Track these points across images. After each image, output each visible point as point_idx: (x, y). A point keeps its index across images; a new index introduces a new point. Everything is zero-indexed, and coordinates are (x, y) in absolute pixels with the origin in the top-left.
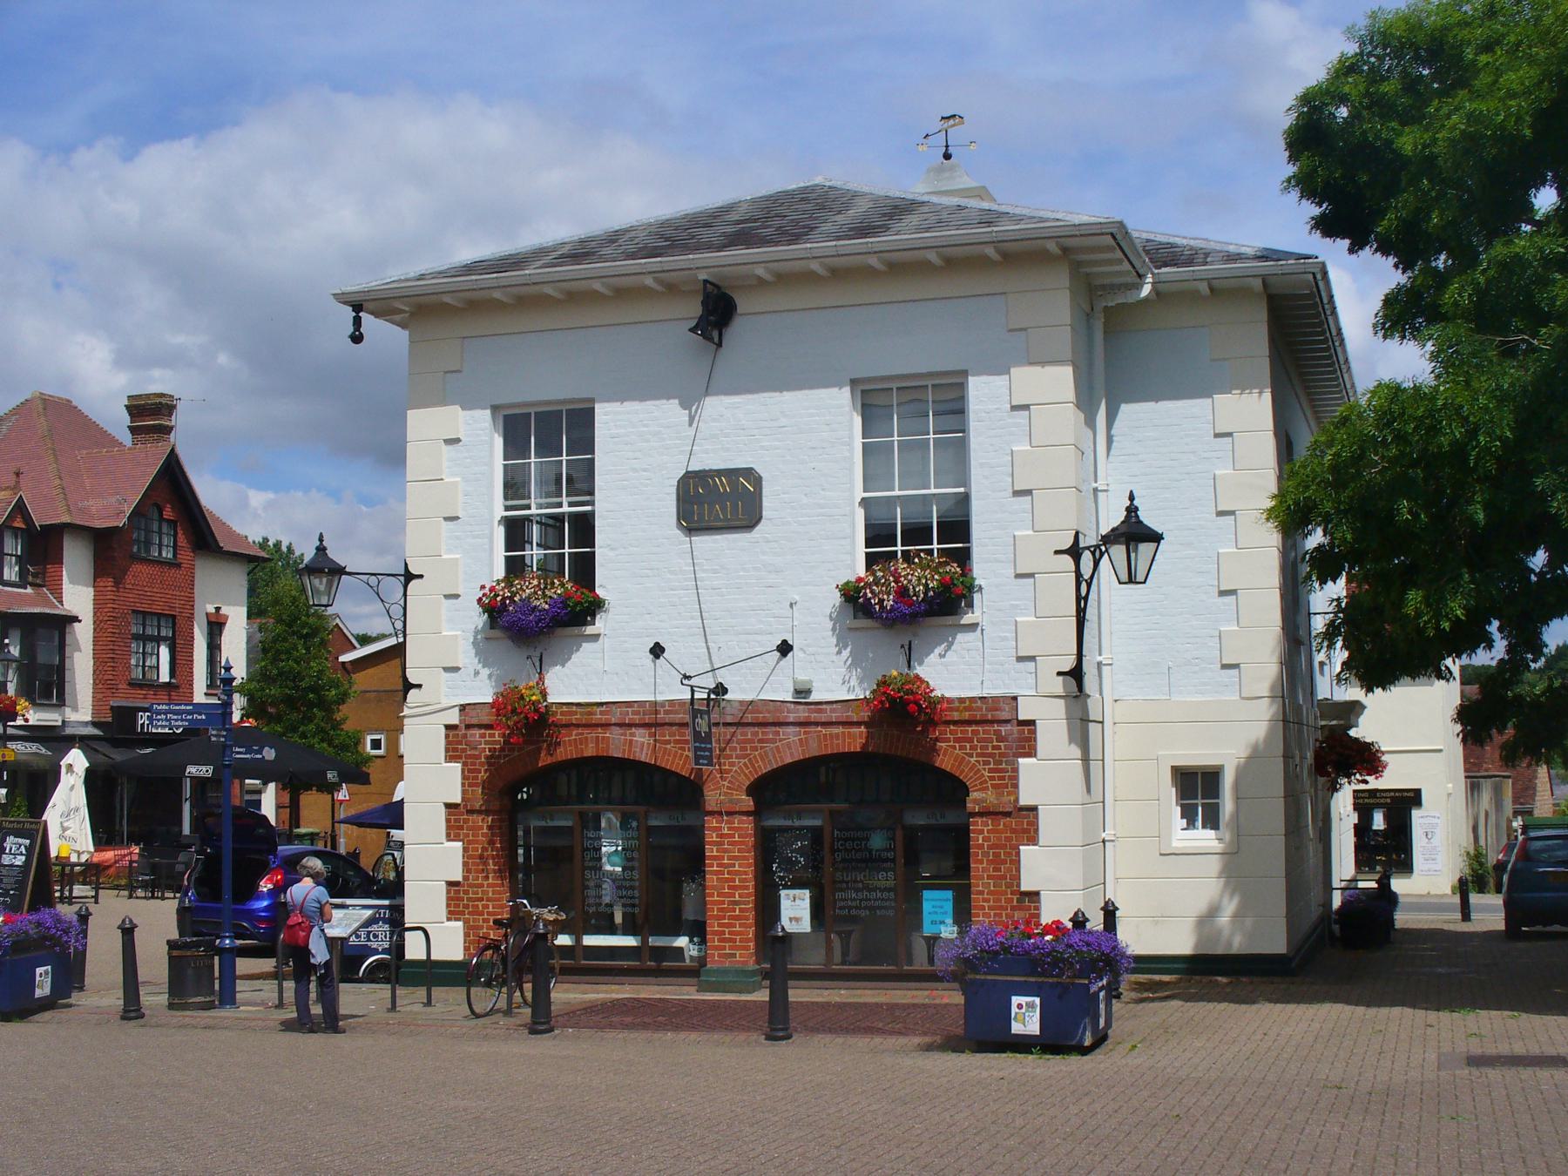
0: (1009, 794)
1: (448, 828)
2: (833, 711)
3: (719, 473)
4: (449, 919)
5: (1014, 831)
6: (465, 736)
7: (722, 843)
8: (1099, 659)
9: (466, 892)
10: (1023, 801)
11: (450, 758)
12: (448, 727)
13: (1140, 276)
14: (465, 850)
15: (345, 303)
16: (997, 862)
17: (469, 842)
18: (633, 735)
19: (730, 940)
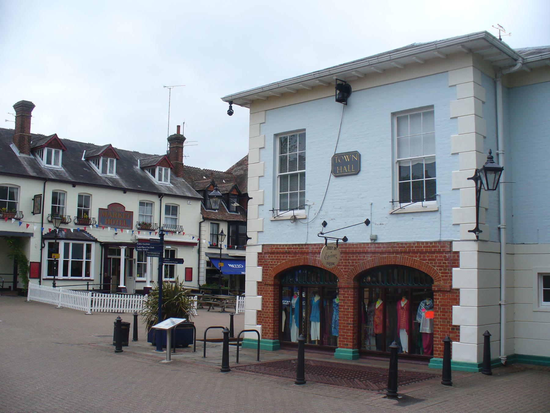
3: (346, 154)
5: (451, 299)
6: (264, 257)
8: (499, 226)
13: (516, 60)
14: (263, 299)
15: (226, 101)
16: (444, 312)
17: (265, 296)
18: (316, 257)
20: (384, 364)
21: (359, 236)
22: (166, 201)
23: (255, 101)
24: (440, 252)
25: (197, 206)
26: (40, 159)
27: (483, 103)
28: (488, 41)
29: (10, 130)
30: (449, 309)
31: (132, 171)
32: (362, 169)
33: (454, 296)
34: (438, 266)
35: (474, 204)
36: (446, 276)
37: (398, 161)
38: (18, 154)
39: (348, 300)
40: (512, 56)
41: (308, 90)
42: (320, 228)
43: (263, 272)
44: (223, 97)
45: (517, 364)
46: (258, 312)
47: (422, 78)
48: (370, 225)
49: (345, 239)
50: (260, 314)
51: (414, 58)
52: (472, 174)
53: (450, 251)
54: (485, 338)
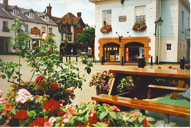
15: (93, 2)
22: (49, 27)
25: (57, 28)
26: (12, 13)
29: (2, 4)
31: (38, 18)
33: (149, 48)
38: (5, 11)
49: (122, 36)
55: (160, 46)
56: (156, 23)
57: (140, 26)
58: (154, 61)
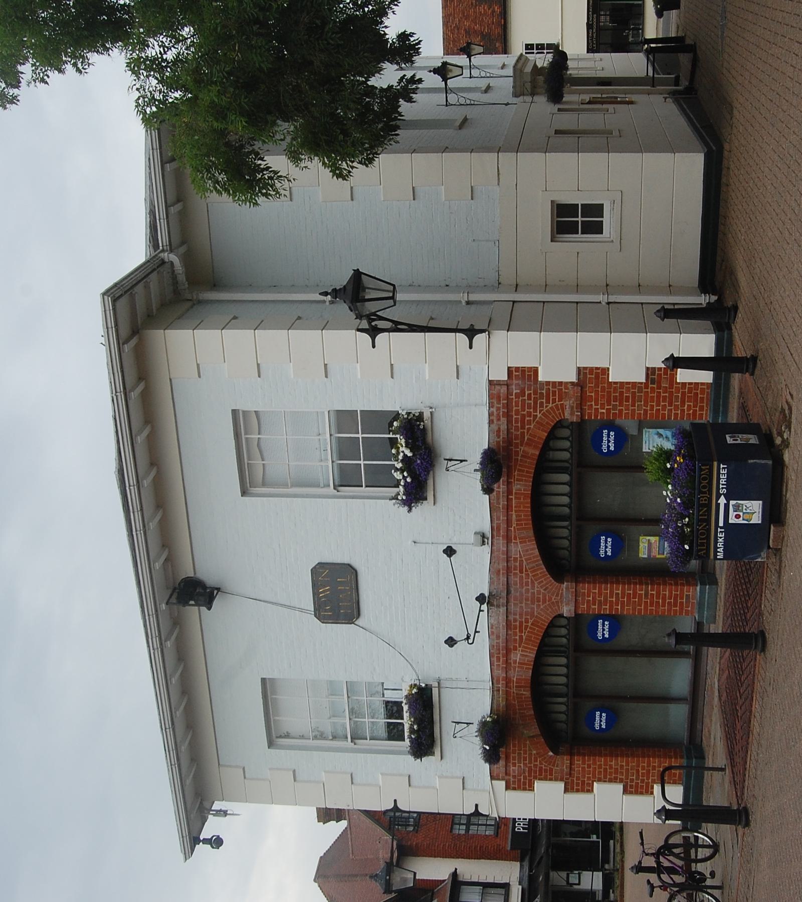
0: (566, 388)
1: (583, 791)
2: (498, 519)
3: (315, 593)
4: (652, 793)
5: (597, 386)
6: (514, 777)
7: (600, 602)
8: (464, 303)
9: (632, 780)
10: (574, 379)
11: (531, 788)
12: (507, 788)
13: (163, 262)
14: (599, 780)
15: (192, 851)
16: (621, 399)
17: (594, 776)
18: (515, 662)
19: (676, 599)
20: (714, 657)
21: (477, 570)
23: (197, 798)
24: (508, 406)
27: (235, 318)
28: (121, 295)
30: (615, 389)
32: (346, 560)
33: (592, 378)
34: (535, 410)
35: (421, 335)
36: (554, 393)
37: (335, 489)
39: (600, 594)
40: (153, 267)
41: (185, 666)
42: (461, 646)
43: (545, 779)
44: (182, 856)
45: (714, 266)
46: (625, 791)
47: (179, 426)
48: (454, 547)
50: (631, 787)
51: (179, 713)
52: (366, 337)
53: (507, 385)
54: (677, 102)
55: (565, 289)
56: (381, 324)
57: (405, 454)
58: (702, 344)
